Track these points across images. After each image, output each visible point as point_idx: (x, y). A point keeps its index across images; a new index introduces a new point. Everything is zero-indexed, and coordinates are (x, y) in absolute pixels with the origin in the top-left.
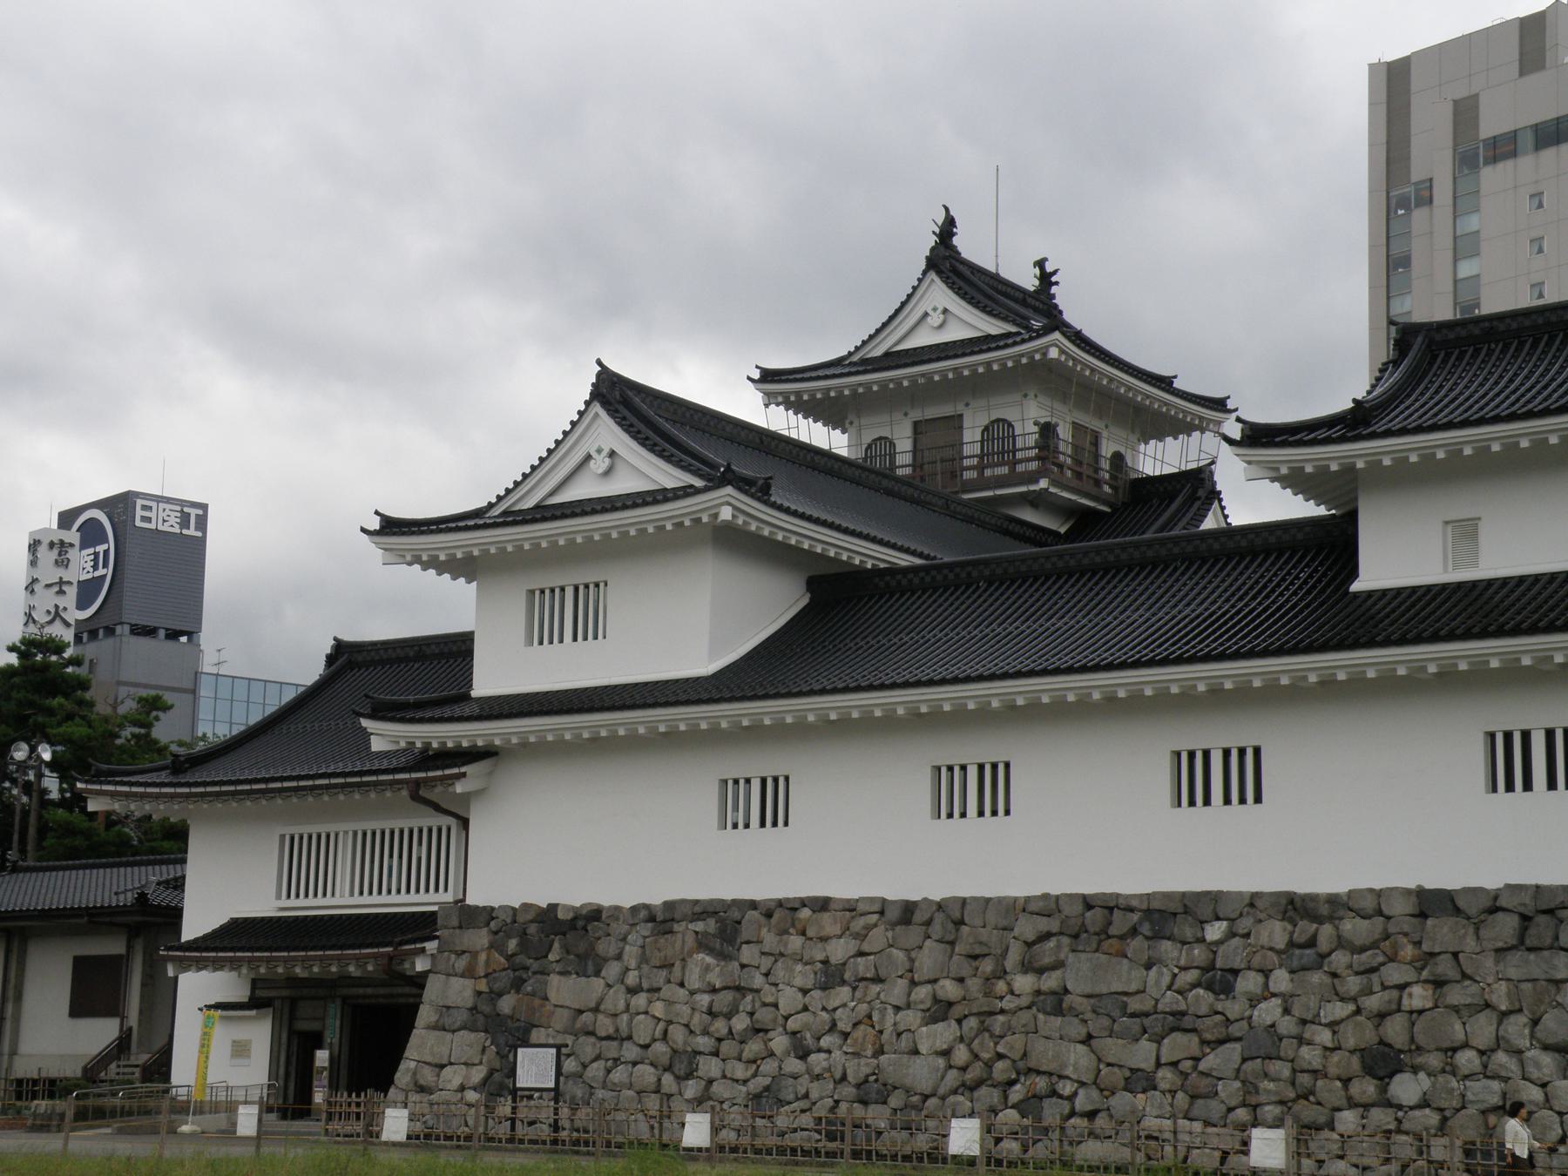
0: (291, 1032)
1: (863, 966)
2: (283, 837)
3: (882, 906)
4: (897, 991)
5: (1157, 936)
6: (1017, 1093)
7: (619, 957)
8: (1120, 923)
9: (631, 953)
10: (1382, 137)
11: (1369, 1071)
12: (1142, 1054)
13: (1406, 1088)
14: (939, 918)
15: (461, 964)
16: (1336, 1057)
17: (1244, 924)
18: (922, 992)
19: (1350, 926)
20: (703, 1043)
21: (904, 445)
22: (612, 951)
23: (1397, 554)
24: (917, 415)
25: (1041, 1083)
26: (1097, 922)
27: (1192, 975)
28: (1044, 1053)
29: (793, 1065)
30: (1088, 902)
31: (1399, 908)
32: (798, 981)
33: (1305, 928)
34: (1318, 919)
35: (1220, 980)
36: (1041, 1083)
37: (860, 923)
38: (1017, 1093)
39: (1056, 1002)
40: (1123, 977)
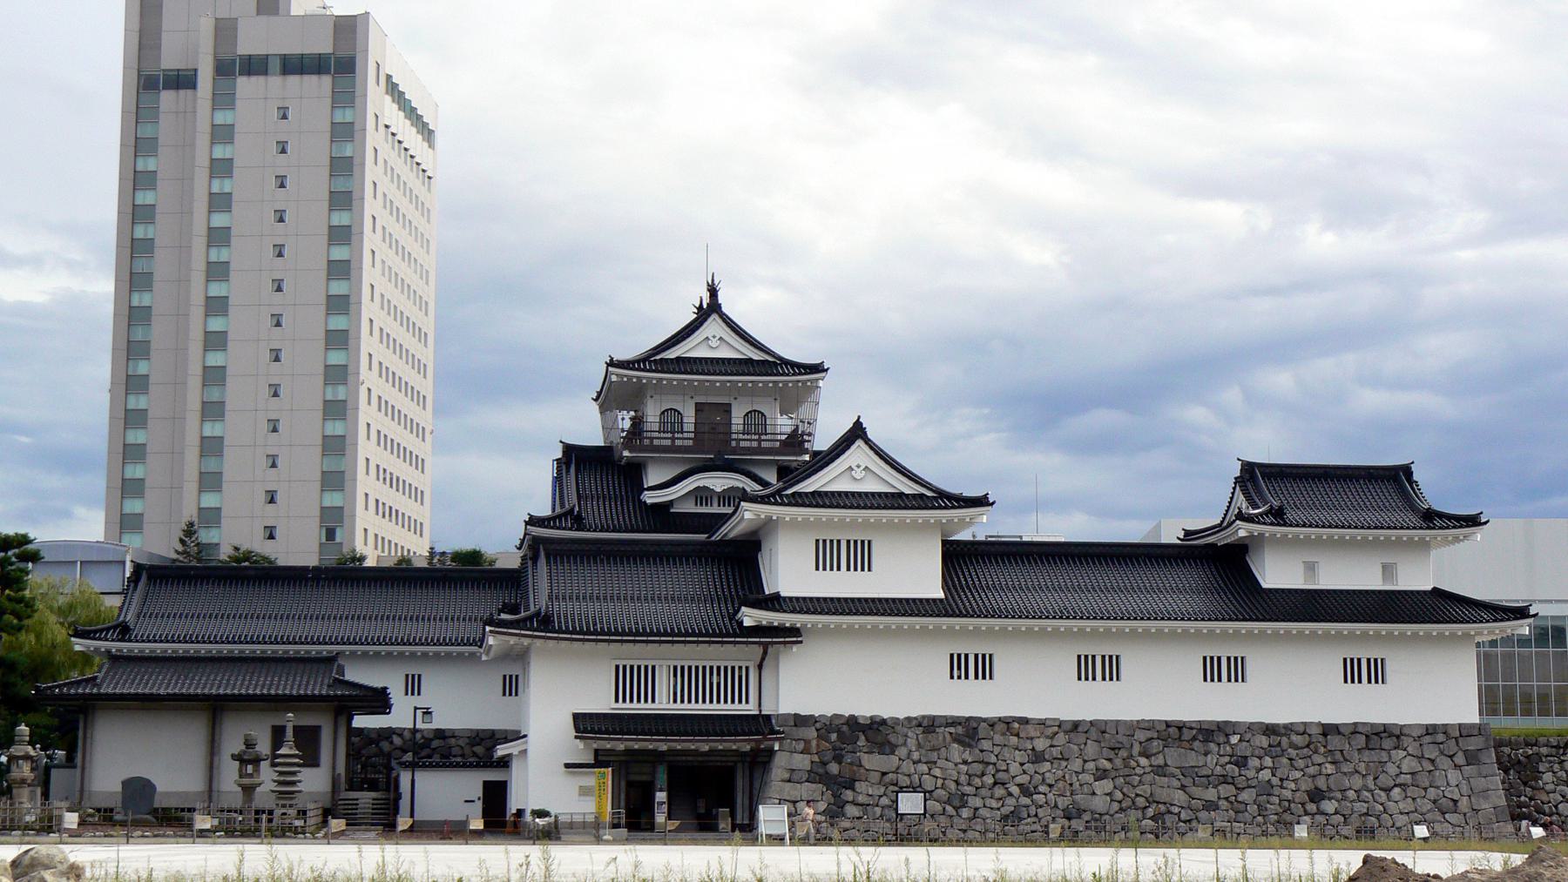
0: (630, 784)
1: (1055, 752)
2: (617, 667)
3: (1060, 724)
4: (1077, 765)
5: (1206, 741)
6: (1150, 812)
7: (905, 744)
8: (1187, 735)
9: (912, 743)
10: (136, 27)
11: (1312, 801)
12: (1211, 794)
13: (1329, 806)
14: (1093, 729)
15: (801, 746)
16: (1298, 794)
17: (1247, 737)
18: (1091, 765)
19: (1294, 738)
20: (968, 790)
21: (689, 418)
22: (901, 741)
23: (1277, 572)
24: (702, 399)
25: (1162, 808)
26: (1174, 733)
27: (1227, 759)
28: (1162, 794)
29: (1025, 801)
30: (1168, 724)
31: (1315, 731)
32: (1018, 759)
33: (1275, 739)
34: (1281, 735)
35: (1241, 762)
36: (1162, 808)
37: (1050, 731)
38: (1150, 812)
39: (1160, 771)
40: (1193, 759)
